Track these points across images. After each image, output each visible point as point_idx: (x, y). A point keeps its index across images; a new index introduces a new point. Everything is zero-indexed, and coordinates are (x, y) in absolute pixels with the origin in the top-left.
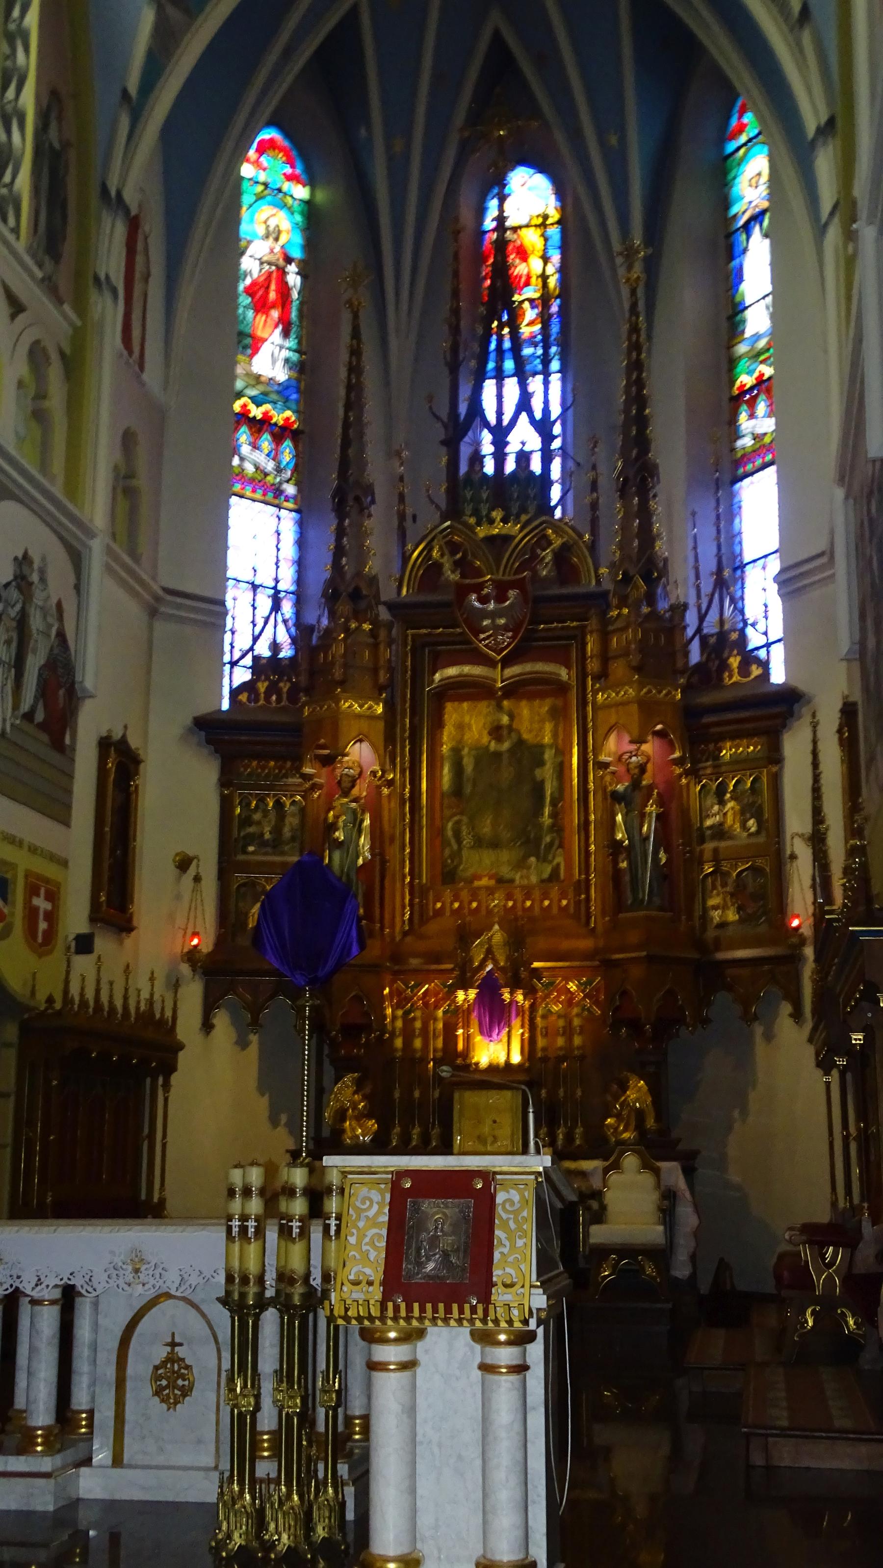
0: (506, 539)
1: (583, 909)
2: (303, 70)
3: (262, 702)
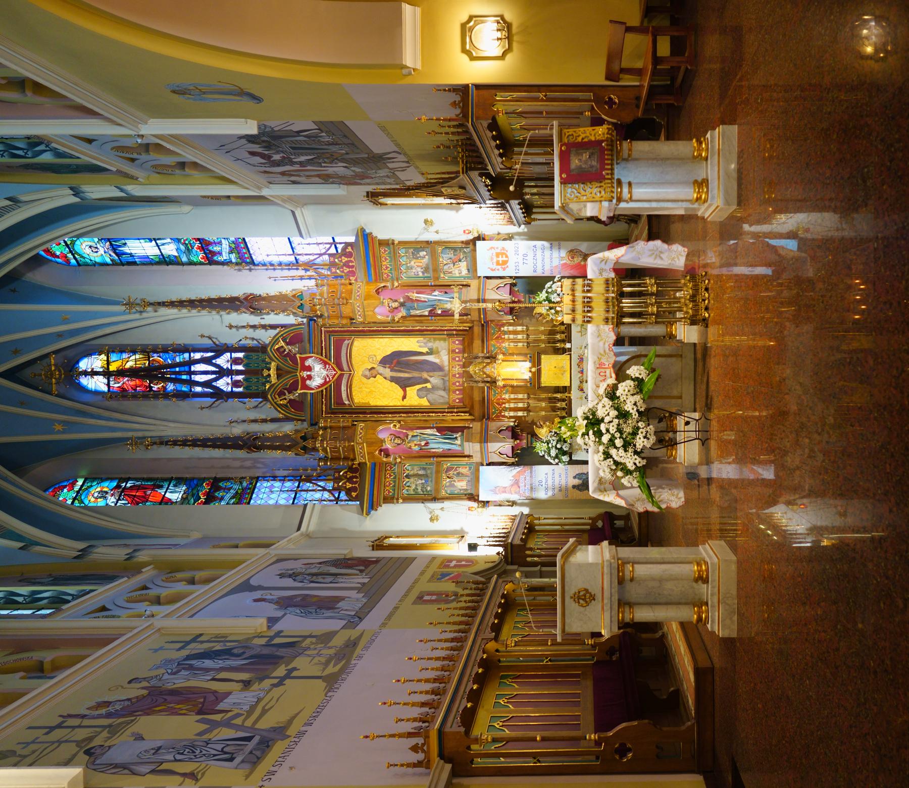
0: (278, 369)
1: (460, 333)
2: (14, 473)
3: (357, 485)
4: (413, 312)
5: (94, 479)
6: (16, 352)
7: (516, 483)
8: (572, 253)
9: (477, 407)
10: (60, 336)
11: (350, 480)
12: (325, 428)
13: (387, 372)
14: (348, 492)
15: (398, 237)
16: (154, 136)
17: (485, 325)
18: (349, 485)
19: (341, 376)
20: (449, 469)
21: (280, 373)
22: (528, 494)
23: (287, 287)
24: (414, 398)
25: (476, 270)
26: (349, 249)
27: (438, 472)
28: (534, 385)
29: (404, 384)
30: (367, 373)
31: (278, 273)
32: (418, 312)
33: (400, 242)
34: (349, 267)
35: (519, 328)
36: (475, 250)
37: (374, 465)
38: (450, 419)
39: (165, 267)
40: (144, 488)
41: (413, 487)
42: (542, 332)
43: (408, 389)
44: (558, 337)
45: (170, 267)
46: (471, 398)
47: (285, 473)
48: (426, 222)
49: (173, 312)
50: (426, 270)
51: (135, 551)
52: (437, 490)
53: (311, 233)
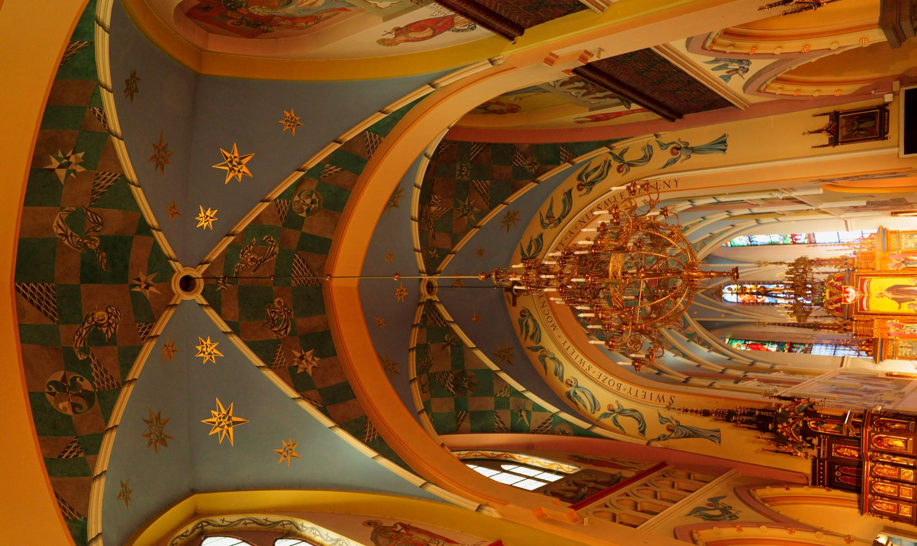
0: (830, 292)
4: (909, 266)
5: (733, 339)
11: (868, 346)
12: (856, 321)
13: (890, 295)
14: (867, 352)
15: (901, 229)
16: (585, 117)
18: (867, 349)
19: (863, 297)
21: (831, 294)
23: (837, 254)
24: (905, 308)
29: (900, 301)
30: (878, 295)
31: (829, 248)
32: (912, 266)
33: (903, 232)
34: (872, 244)
39: (771, 246)
43: (902, 304)
45: (774, 246)
47: (828, 342)
51: (774, 365)
53: (849, 227)
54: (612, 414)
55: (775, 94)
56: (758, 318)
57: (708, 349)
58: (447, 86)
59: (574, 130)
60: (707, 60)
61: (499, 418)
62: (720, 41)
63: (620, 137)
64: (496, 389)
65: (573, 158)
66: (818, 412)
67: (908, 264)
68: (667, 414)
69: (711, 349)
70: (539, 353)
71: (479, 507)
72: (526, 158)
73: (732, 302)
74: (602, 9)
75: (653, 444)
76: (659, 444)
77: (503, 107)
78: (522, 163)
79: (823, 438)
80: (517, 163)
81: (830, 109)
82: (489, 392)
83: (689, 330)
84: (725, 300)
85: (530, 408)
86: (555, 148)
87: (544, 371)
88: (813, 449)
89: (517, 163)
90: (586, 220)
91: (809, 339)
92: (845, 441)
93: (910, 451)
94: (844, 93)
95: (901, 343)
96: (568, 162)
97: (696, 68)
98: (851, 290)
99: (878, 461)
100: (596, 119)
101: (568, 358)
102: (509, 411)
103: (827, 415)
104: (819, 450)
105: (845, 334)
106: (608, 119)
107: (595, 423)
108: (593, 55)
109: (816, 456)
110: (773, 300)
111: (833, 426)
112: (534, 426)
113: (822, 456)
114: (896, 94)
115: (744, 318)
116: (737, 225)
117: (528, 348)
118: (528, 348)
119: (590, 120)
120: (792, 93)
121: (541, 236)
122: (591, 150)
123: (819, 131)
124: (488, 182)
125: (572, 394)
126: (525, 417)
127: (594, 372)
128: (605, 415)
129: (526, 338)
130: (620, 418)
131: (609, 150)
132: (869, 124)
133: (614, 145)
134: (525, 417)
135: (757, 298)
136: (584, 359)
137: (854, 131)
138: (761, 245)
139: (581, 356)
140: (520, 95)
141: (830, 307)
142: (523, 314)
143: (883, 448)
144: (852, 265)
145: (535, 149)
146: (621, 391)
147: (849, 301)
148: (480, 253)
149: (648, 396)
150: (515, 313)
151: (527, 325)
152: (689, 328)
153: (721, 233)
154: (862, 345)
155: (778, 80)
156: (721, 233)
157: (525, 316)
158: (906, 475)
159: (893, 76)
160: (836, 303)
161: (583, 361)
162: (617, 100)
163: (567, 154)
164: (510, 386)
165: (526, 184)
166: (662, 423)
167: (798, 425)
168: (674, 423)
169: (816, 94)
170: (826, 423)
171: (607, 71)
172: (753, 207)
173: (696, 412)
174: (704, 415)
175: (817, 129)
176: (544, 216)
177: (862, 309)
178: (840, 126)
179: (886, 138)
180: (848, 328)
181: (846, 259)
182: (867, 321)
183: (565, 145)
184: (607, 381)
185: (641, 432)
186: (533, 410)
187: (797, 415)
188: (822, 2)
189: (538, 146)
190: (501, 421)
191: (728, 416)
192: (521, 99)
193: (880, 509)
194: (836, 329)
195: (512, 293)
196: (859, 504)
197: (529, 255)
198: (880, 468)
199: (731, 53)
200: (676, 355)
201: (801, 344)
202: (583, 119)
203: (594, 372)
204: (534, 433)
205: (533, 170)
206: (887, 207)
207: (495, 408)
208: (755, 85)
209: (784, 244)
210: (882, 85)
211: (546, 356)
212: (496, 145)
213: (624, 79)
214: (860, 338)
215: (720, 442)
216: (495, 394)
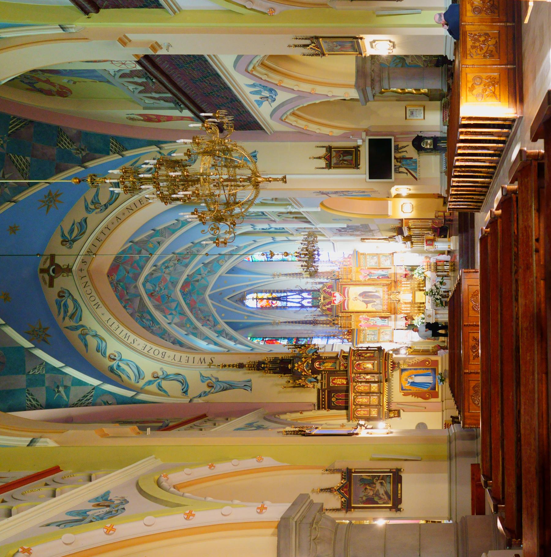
0: (324, 297)
5: (254, 338)
6: (234, 291)
7: (407, 336)
8: (426, 257)
9: (393, 310)
10: (247, 286)
12: (341, 317)
13: (361, 298)
14: (348, 339)
16: (136, 115)
17: (395, 282)
18: (348, 337)
19: (345, 300)
20: (383, 332)
21: (325, 298)
22: (411, 340)
24: (370, 308)
25: (393, 263)
26: (350, 256)
27: (379, 333)
28: (413, 303)
29: (367, 303)
30: (354, 299)
32: (373, 277)
33: (368, 254)
35: (408, 283)
36: (393, 256)
37: (357, 330)
38: (383, 315)
39: (282, 262)
40: (272, 340)
41: (370, 338)
42: (416, 284)
44: (421, 285)
46: (391, 307)
48: (377, 247)
49: (284, 278)
50: (376, 263)
52: (379, 338)
54: (155, 381)
55: (292, 125)
56: (273, 319)
57: (235, 342)
58: (6, 38)
59: (124, 126)
60: (248, 84)
61: (32, 395)
62: (259, 69)
63: (168, 140)
64: (29, 367)
65: (123, 151)
66: (321, 355)
67: (372, 276)
68: (207, 373)
69: (237, 343)
70: (79, 332)
71: (31, 442)
72: (73, 143)
73: (252, 308)
74: (175, 12)
75: (196, 401)
76: (200, 400)
77: (52, 88)
78: (68, 147)
79: (324, 373)
80: (62, 145)
81: (327, 144)
82: (20, 369)
83: (219, 327)
84: (247, 306)
85: (69, 384)
86: (105, 139)
87: (85, 349)
88: (318, 382)
89: (62, 145)
90: (134, 207)
91: (310, 334)
92: (338, 374)
93: (376, 370)
94: (334, 135)
95: (368, 332)
96: (118, 153)
97: (240, 88)
98: (337, 294)
99: (358, 382)
100: (148, 119)
101: (112, 334)
102: (44, 388)
103: (327, 357)
104: (322, 383)
105: (334, 328)
106: (159, 121)
107: (139, 391)
108: (162, 48)
109: (320, 388)
110: (284, 304)
111: (330, 364)
112: (73, 399)
113: (323, 387)
114: (364, 141)
115: (263, 319)
116: (258, 241)
117: (67, 328)
118: (67, 328)
119: (142, 118)
120: (303, 127)
121: (85, 220)
122: (141, 147)
123: (320, 158)
124: (28, 158)
125: (115, 368)
126: (63, 392)
127: (139, 345)
128: (150, 383)
129: (64, 318)
130: (164, 384)
131: (158, 149)
132: (348, 158)
133: (163, 145)
134: (63, 392)
135: (272, 303)
136: (129, 333)
137: (341, 161)
138: (275, 261)
139: (126, 331)
140: (75, 79)
141: (324, 308)
142: (61, 294)
143: (361, 370)
144: (337, 276)
145: (81, 136)
146: (166, 358)
147: (336, 302)
148: (13, 229)
149: (191, 360)
150: (51, 294)
151: (65, 305)
152: (219, 326)
153: (246, 247)
154: (345, 335)
155: (293, 114)
156: (246, 247)
157: (64, 296)
158: (374, 388)
159: (363, 129)
160: (327, 305)
161: (128, 335)
162: (172, 105)
163: (116, 147)
164: (46, 363)
165: (72, 167)
166: (203, 382)
167: (308, 363)
168: (214, 380)
169: (318, 131)
170: (326, 363)
171: (167, 72)
172: (271, 223)
173: (233, 366)
174: (239, 368)
175: (318, 156)
176: (89, 201)
177: (344, 309)
178: (332, 156)
179: (359, 168)
180: (336, 322)
181: (334, 272)
182: (348, 317)
183: (116, 138)
184: (152, 351)
185: (184, 393)
186: (72, 385)
187: (307, 355)
188: (325, 53)
189: (86, 134)
190: (34, 399)
191: (258, 366)
192: (75, 83)
193: (360, 415)
194: (328, 324)
195: (49, 274)
196: (347, 416)
197: (70, 238)
198: (359, 386)
199: (265, 80)
200: (209, 344)
201: (304, 338)
202: (136, 117)
203: (139, 345)
204: (72, 407)
205: (80, 155)
206: (358, 233)
207: (27, 386)
208: (279, 113)
209: (292, 261)
210: (355, 133)
211: (87, 334)
212: (39, 124)
213: (181, 83)
214: (344, 330)
215: (251, 390)
216: (27, 371)
